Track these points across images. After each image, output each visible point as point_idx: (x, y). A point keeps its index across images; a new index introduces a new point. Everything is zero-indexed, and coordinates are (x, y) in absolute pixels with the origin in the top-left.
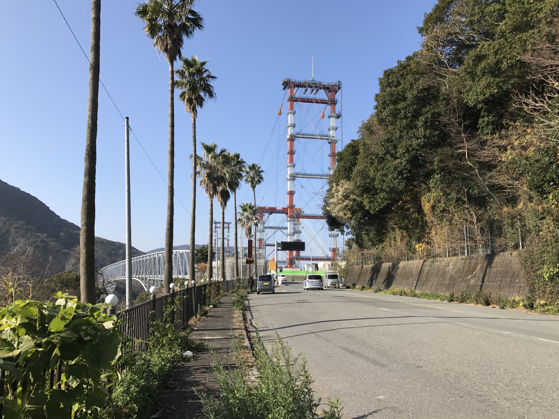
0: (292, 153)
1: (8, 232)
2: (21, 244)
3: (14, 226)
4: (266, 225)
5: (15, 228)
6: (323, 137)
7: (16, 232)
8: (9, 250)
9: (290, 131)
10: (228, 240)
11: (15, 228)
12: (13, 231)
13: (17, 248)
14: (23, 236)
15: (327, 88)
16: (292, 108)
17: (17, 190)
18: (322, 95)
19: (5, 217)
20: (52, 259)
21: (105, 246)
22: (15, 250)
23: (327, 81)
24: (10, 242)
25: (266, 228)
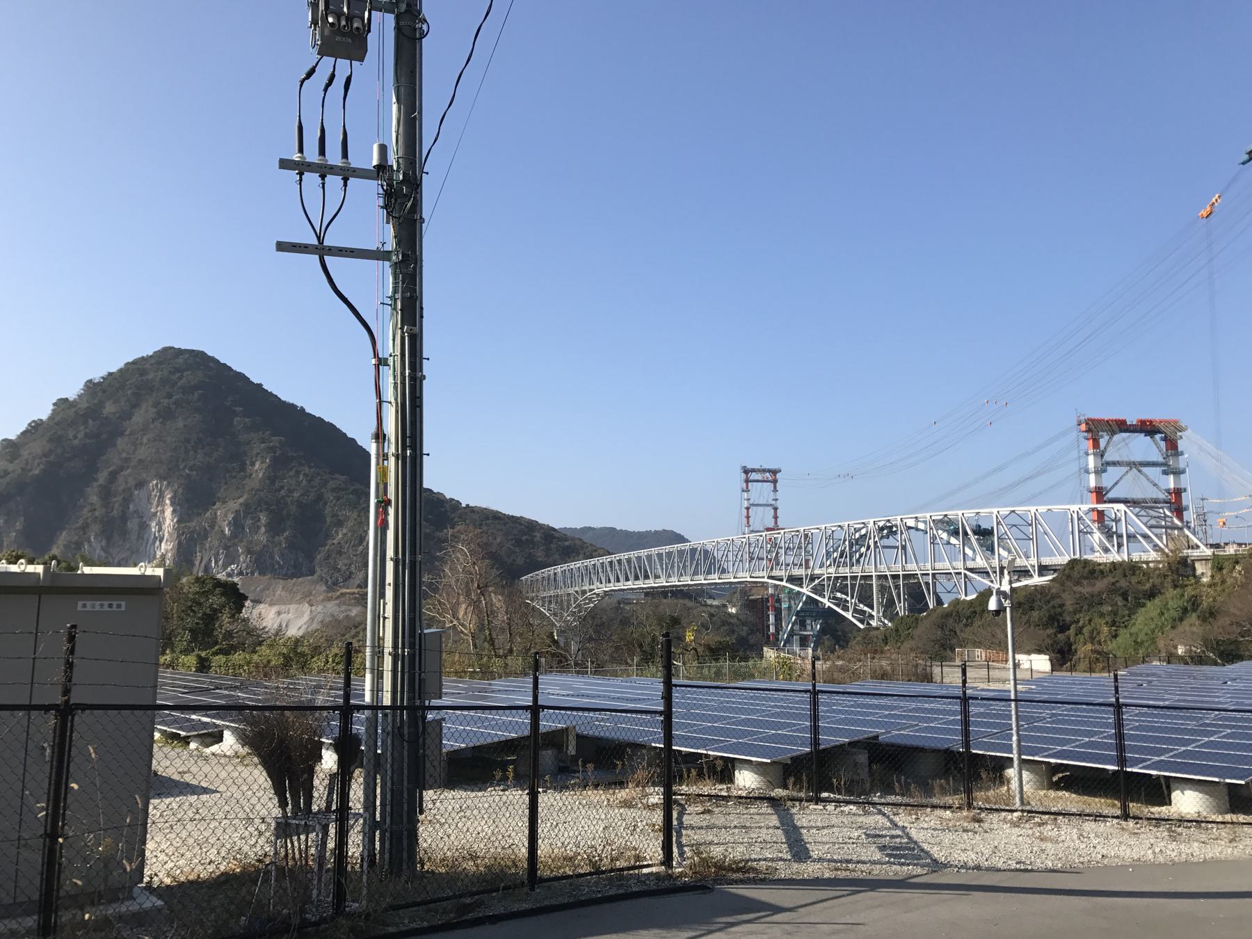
0: (748, 517)
1: (320, 497)
2: (350, 524)
3: (331, 485)
5: (333, 490)
7: (338, 499)
8: (328, 536)
9: (746, 504)
10: (776, 509)
11: (333, 490)
12: (330, 496)
15: (769, 471)
17: (242, 377)
19: (310, 468)
21: (505, 524)
25: (1108, 464)
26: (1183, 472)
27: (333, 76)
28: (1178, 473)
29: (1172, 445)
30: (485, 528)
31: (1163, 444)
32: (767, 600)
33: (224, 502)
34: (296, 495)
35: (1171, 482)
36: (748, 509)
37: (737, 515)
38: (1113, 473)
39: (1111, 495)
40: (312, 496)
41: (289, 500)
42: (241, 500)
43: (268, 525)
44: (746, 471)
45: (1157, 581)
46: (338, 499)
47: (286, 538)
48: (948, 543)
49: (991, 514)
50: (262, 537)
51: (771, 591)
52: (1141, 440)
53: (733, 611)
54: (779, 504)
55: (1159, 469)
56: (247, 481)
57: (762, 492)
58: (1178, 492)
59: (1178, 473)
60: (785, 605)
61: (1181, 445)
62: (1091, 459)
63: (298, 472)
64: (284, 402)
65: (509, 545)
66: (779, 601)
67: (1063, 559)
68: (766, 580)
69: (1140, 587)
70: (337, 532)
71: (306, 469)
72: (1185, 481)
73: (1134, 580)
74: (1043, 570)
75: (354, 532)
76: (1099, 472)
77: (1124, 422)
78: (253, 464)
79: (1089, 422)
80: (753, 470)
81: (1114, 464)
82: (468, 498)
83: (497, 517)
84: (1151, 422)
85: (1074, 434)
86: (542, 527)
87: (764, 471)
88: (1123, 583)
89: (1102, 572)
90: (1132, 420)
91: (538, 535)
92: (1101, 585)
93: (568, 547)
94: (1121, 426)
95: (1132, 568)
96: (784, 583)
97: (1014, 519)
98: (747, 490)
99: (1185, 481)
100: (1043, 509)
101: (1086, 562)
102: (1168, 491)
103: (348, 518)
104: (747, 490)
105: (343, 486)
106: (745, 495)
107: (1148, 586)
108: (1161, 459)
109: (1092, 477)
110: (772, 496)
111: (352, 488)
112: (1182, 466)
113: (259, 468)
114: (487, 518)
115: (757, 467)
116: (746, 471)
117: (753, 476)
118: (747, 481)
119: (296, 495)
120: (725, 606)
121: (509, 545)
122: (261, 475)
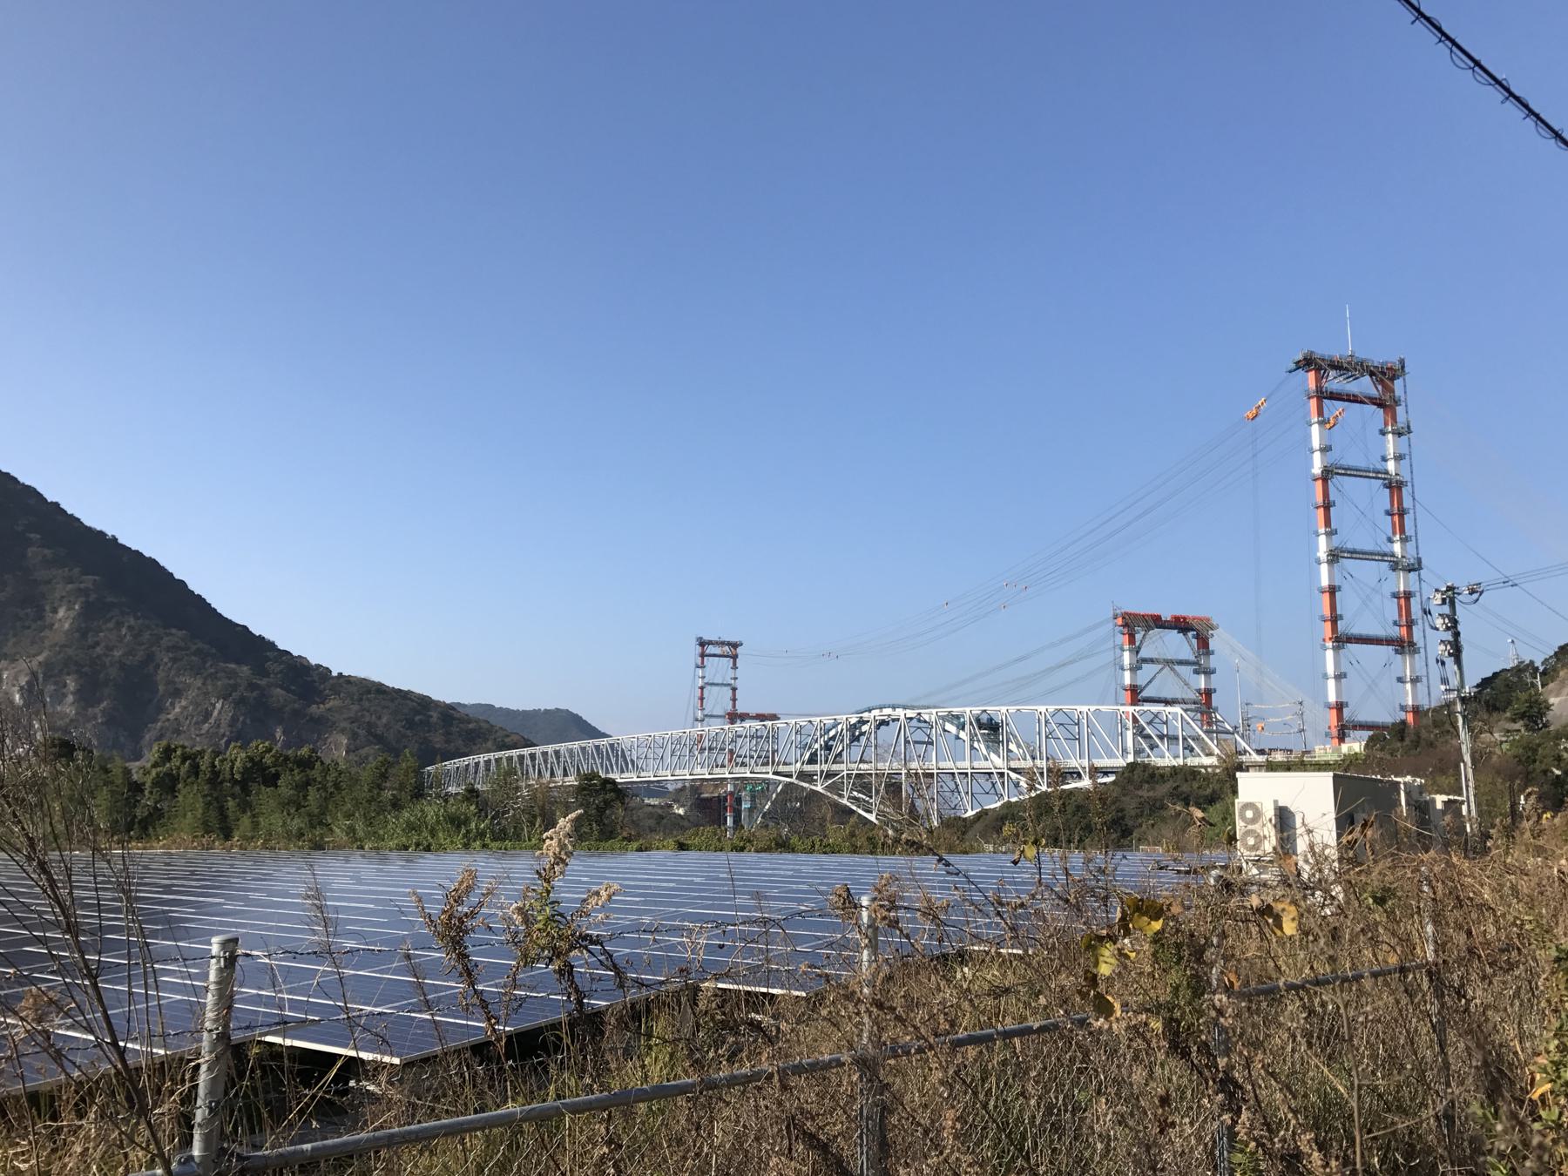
0: (702, 699)
1: (150, 658)
2: (192, 694)
3: (165, 642)
4: (1144, 654)
6: (1379, 474)
7: (174, 660)
8: (160, 709)
9: (700, 683)
10: (734, 690)
11: (168, 649)
13: (184, 703)
14: (196, 671)
15: (729, 644)
16: (1320, 413)
17: (31, 492)
18: (1365, 385)
19: (137, 618)
20: (284, 733)
22: (177, 710)
23: (1379, 356)
24: (161, 688)
25: (1145, 661)
26: (1213, 672)
28: (1208, 672)
29: (1203, 643)
30: (366, 704)
31: (1194, 642)
32: (725, 799)
33: (14, 660)
34: (117, 653)
35: (1202, 682)
36: (702, 688)
37: (690, 696)
38: (1149, 670)
39: (1145, 694)
40: (140, 655)
41: (107, 660)
42: (40, 658)
43: (77, 692)
44: (703, 643)
45: (1217, 787)
46: (174, 660)
47: (103, 712)
48: (958, 738)
49: (1000, 711)
50: (68, 708)
51: (730, 788)
52: (1173, 635)
53: (681, 811)
54: (738, 684)
55: (1190, 668)
56: (47, 633)
57: (718, 668)
58: (1208, 693)
59: (1208, 672)
60: (745, 805)
61: (1212, 644)
62: (1126, 655)
63: (119, 625)
64: (90, 529)
65: (398, 726)
66: (739, 801)
67: (1120, 762)
68: (770, 776)
69: (1201, 792)
70: (173, 704)
71: (132, 621)
73: (1195, 785)
74: (1095, 771)
75: (197, 705)
76: (1134, 669)
77: (1159, 617)
78: (55, 611)
79: (1125, 616)
80: (710, 643)
81: (1152, 661)
82: (339, 665)
83: (380, 689)
85: (1111, 625)
86: (437, 704)
87: (723, 643)
88: (1185, 788)
89: (1162, 776)
90: (1167, 616)
91: (435, 715)
92: (1163, 789)
93: (472, 731)
94: (1157, 622)
95: (1191, 773)
96: (793, 780)
97: (1061, 718)
98: (703, 667)
100: (1093, 708)
101: (1146, 767)
102: (1199, 691)
103: (189, 686)
104: (703, 667)
105: (182, 644)
106: (700, 672)
107: (1209, 791)
108: (1192, 658)
109: (1127, 674)
110: (731, 673)
111: (194, 648)
112: (1212, 666)
113: (64, 617)
114: (369, 692)
115: (714, 638)
116: (703, 643)
117: (711, 649)
118: (703, 655)
119: (117, 653)
120: (671, 806)
121: (398, 726)
122: (67, 626)
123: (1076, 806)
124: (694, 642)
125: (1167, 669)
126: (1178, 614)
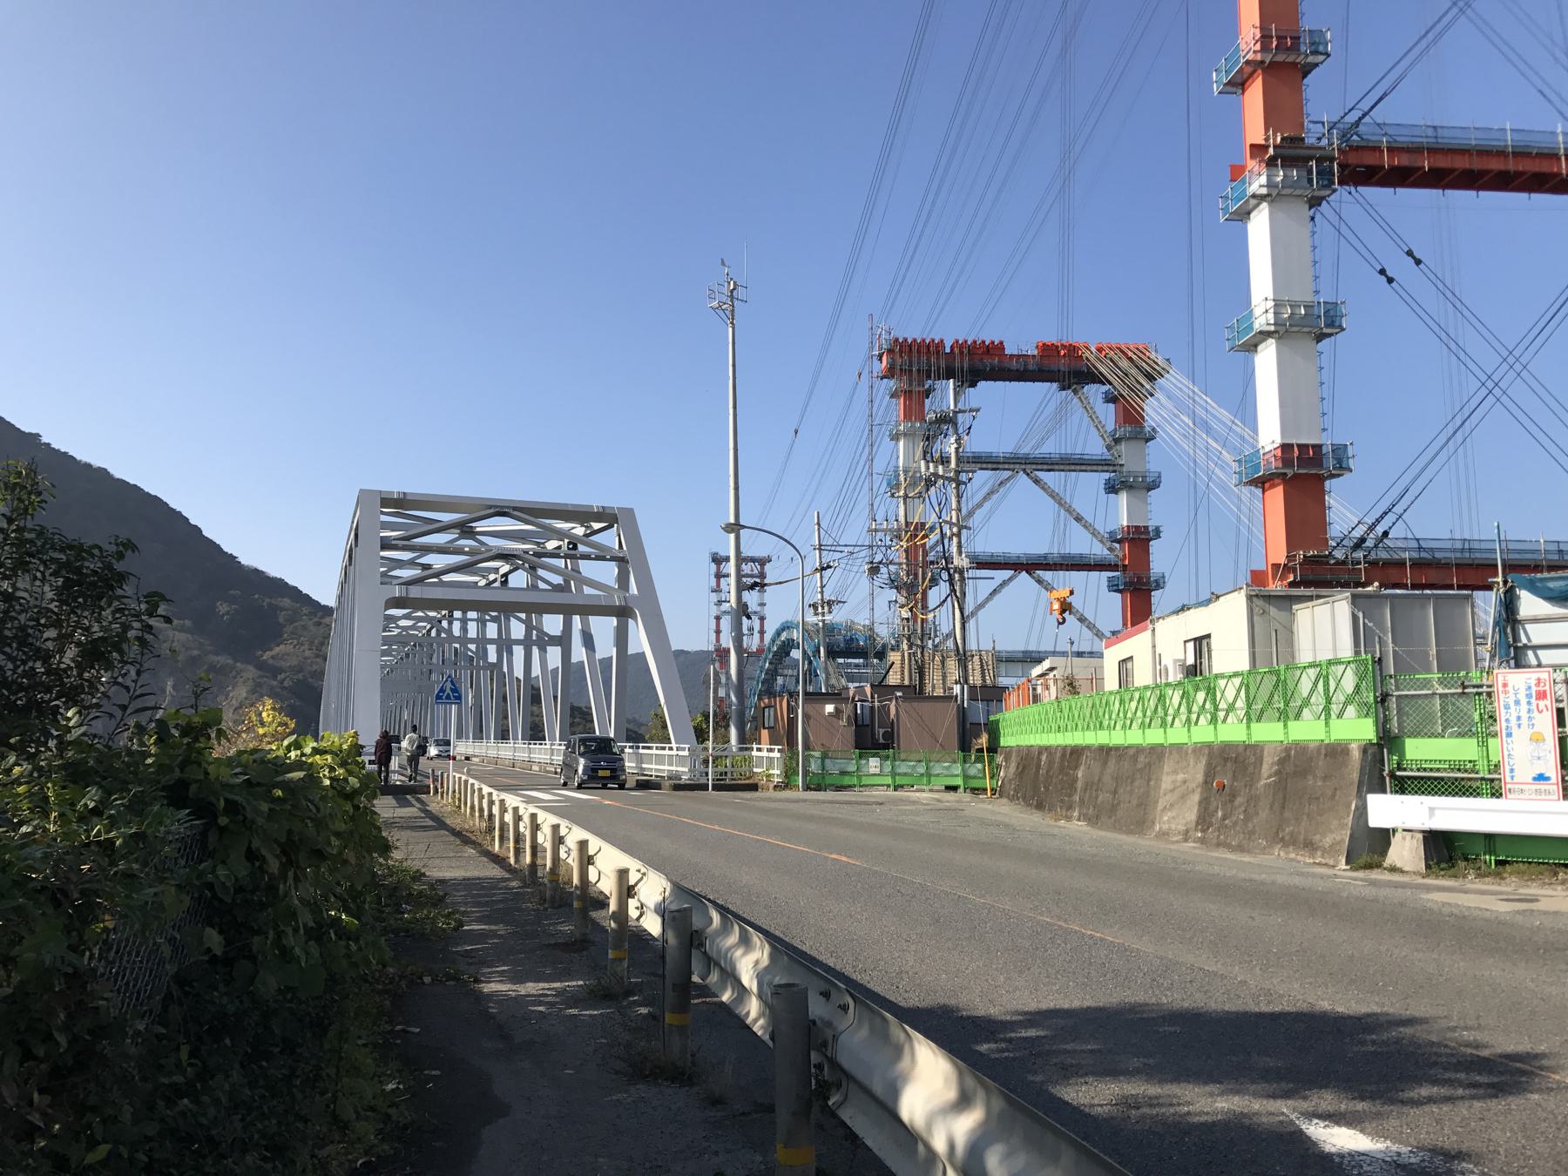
20: (174, 687)
26: (1153, 485)
27: (1541, 92)
55: (1099, 479)
61: (1154, 411)
72: (1159, 510)
84: (1072, 349)
90: (1021, 342)
94: (981, 364)
99: (1159, 510)
108: (1095, 447)
123: (1206, 782)
124: (708, 559)
125: (1022, 476)
126: (1051, 338)
